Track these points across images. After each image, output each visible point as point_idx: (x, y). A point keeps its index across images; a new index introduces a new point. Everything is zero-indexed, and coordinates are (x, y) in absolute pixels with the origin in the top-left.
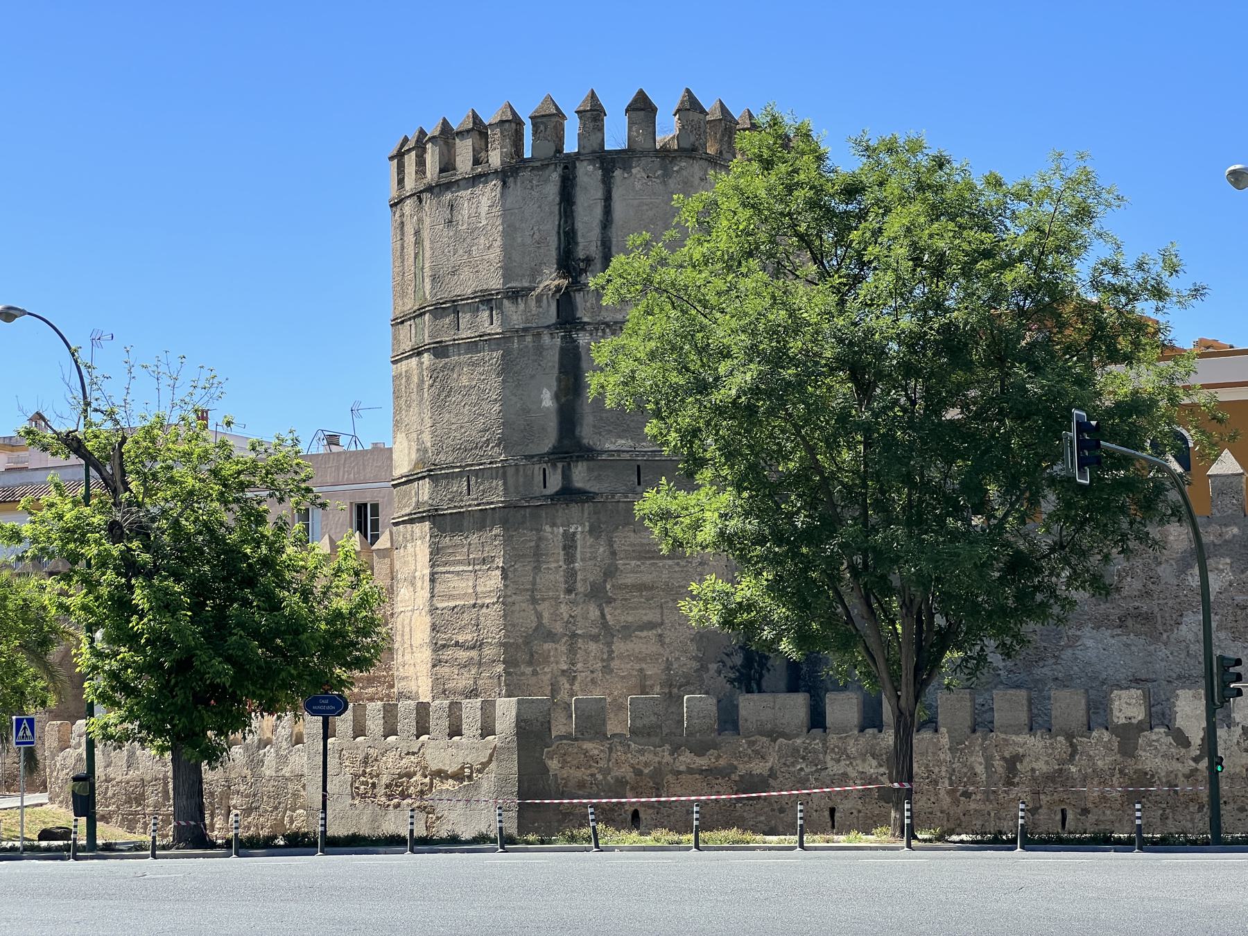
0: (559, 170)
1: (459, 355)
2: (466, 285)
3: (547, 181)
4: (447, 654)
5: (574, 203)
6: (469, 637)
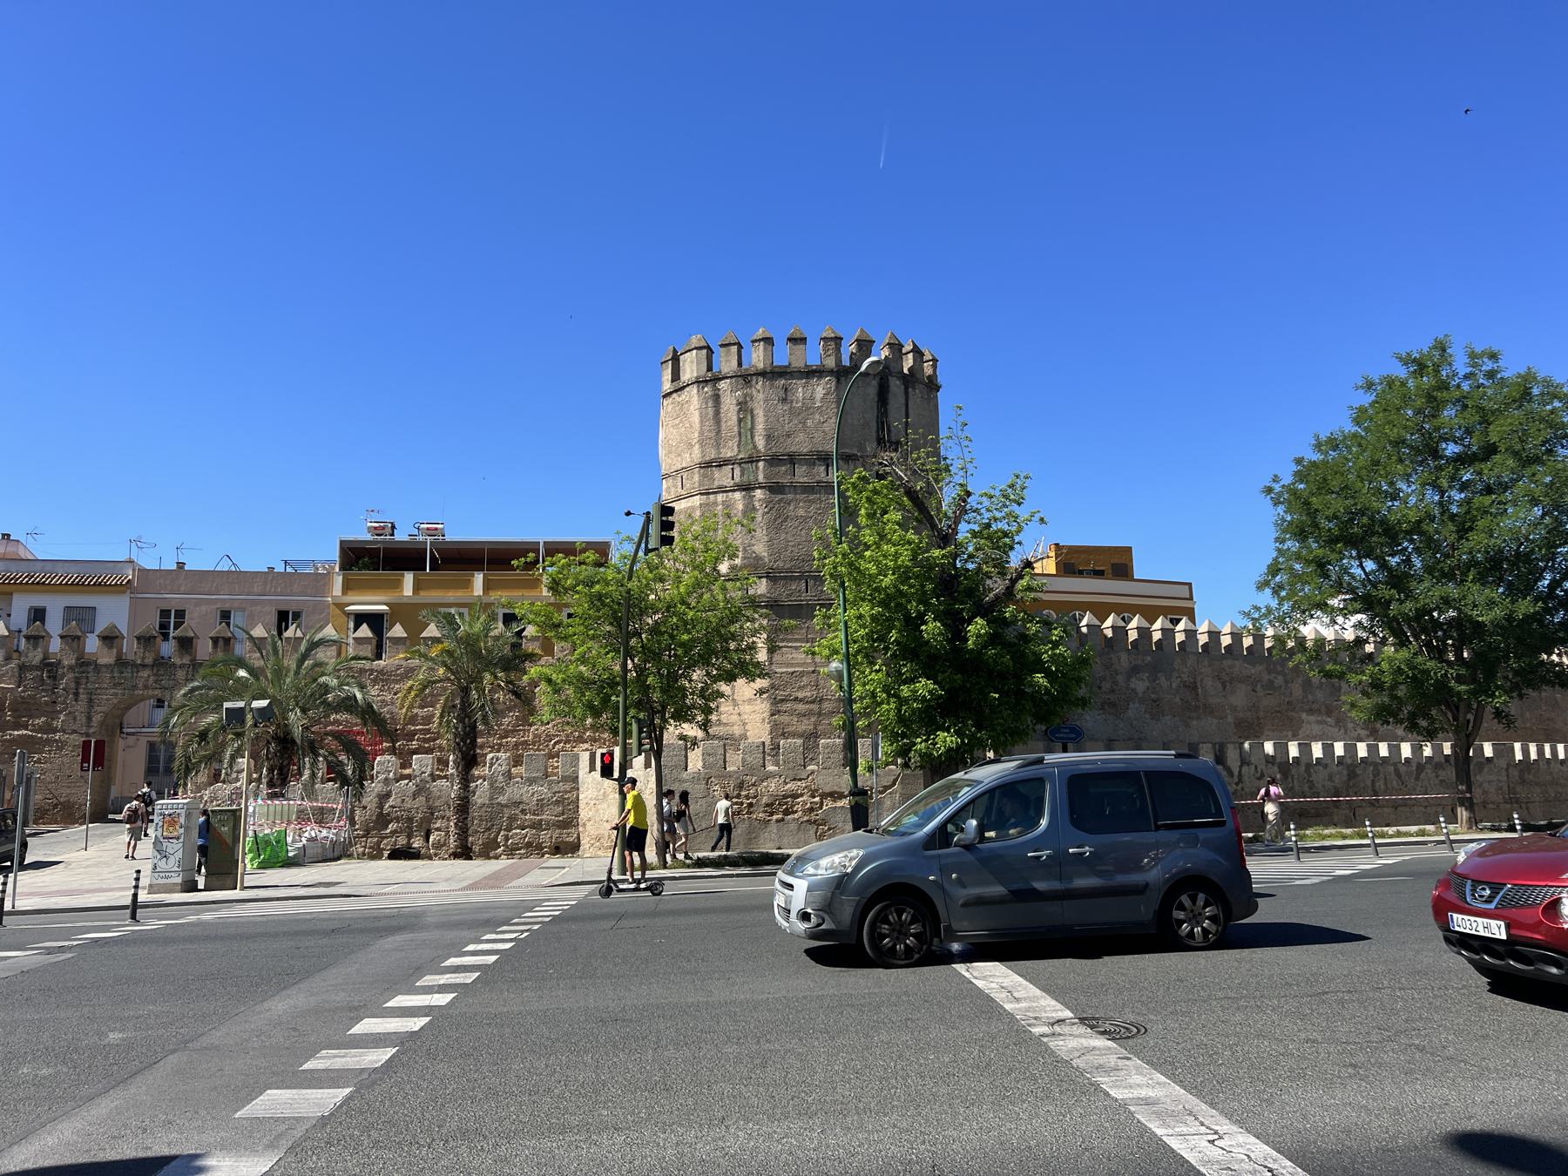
2: (800, 444)
4: (785, 707)
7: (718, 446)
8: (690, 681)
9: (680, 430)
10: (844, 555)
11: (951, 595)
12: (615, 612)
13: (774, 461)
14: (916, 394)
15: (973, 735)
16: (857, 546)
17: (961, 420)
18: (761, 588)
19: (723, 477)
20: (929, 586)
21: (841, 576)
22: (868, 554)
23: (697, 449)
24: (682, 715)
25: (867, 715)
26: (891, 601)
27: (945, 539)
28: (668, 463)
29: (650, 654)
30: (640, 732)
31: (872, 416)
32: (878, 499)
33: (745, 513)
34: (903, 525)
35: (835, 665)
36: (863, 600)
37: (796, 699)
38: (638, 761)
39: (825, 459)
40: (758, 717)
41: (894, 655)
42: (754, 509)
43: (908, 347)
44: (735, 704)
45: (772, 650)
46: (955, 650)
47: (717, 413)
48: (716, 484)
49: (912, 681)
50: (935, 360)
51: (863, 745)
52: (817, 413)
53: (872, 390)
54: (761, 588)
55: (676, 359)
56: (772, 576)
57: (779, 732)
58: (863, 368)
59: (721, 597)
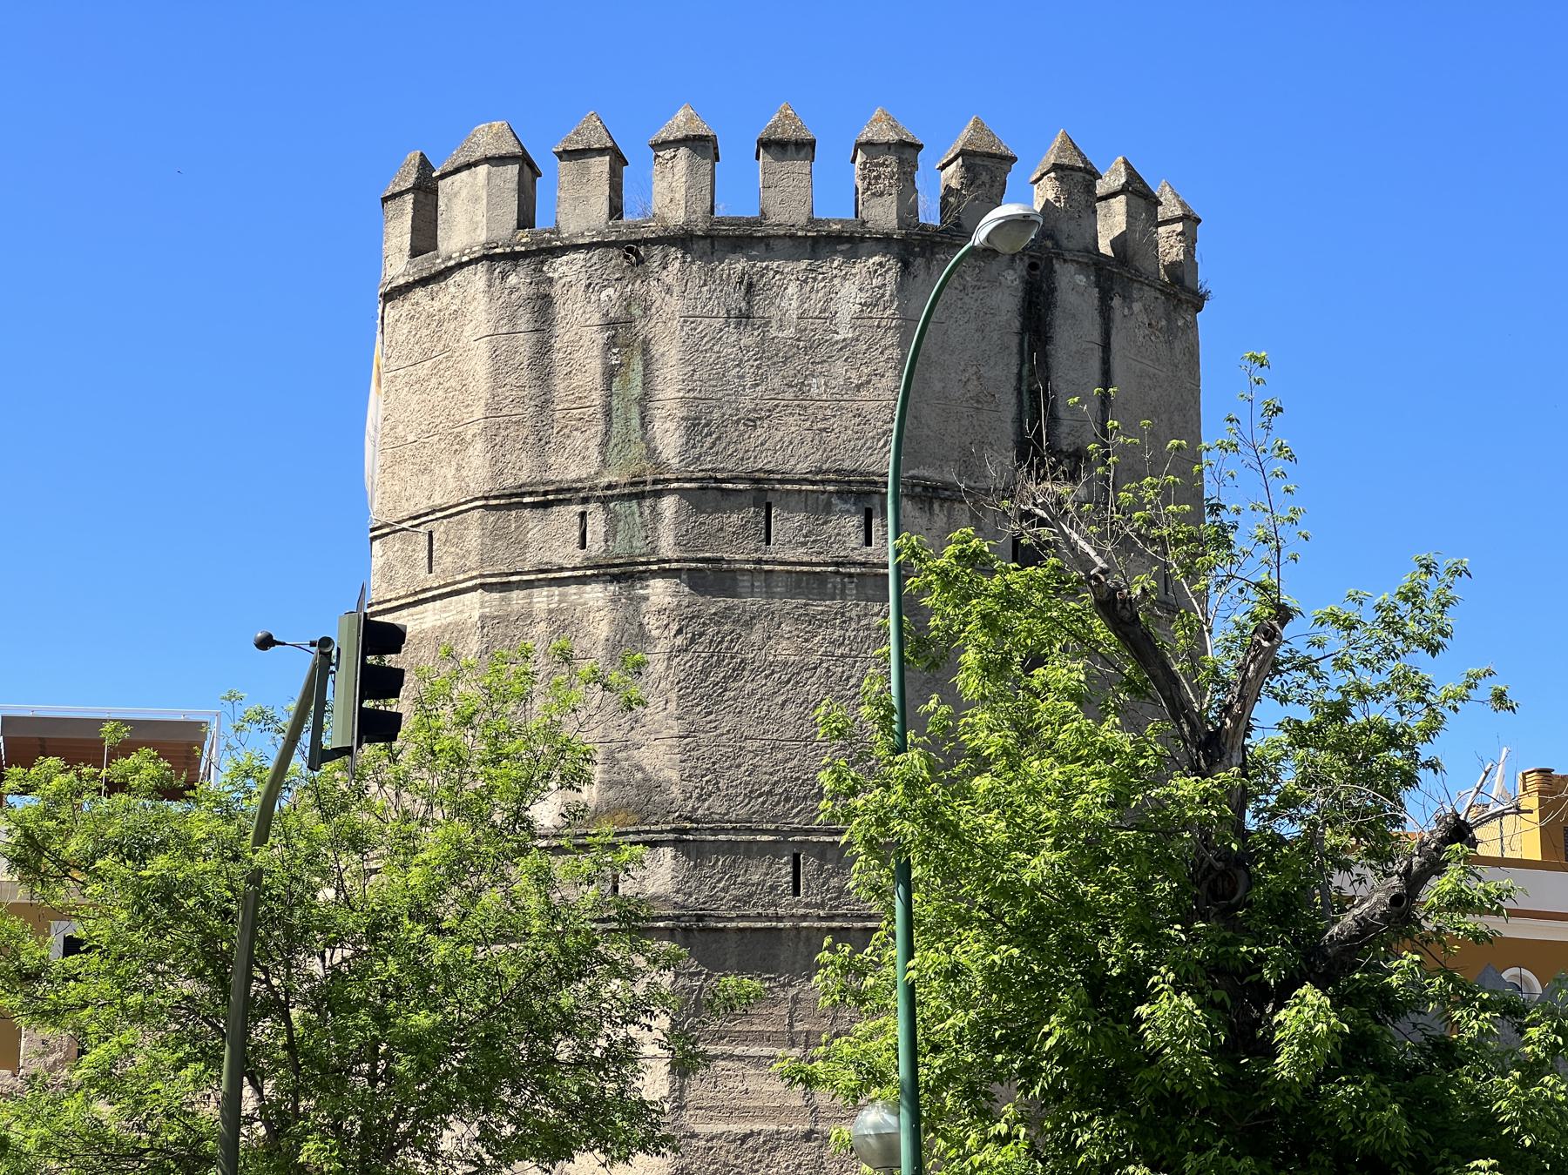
0: (1021, 267)
1: (770, 595)
2: (787, 448)
3: (995, 282)
7: (541, 444)
9: (432, 400)
11: (1226, 914)
12: (210, 939)
13: (708, 494)
14: (1135, 316)
16: (953, 759)
17: (1262, 396)
18: (657, 876)
19: (553, 538)
20: (1163, 887)
21: (900, 848)
22: (982, 783)
26: (1049, 926)
27: (1211, 746)
28: (389, 489)
31: (1003, 371)
36: (964, 921)
39: (860, 494)
41: (1054, 1093)
42: (643, 636)
43: (1112, 178)
47: (543, 349)
48: (531, 559)
50: (1190, 220)
52: (838, 365)
54: (657, 876)
55: (426, 190)
56: (689, 842)
58: (980, 236)
59: (533, 903)
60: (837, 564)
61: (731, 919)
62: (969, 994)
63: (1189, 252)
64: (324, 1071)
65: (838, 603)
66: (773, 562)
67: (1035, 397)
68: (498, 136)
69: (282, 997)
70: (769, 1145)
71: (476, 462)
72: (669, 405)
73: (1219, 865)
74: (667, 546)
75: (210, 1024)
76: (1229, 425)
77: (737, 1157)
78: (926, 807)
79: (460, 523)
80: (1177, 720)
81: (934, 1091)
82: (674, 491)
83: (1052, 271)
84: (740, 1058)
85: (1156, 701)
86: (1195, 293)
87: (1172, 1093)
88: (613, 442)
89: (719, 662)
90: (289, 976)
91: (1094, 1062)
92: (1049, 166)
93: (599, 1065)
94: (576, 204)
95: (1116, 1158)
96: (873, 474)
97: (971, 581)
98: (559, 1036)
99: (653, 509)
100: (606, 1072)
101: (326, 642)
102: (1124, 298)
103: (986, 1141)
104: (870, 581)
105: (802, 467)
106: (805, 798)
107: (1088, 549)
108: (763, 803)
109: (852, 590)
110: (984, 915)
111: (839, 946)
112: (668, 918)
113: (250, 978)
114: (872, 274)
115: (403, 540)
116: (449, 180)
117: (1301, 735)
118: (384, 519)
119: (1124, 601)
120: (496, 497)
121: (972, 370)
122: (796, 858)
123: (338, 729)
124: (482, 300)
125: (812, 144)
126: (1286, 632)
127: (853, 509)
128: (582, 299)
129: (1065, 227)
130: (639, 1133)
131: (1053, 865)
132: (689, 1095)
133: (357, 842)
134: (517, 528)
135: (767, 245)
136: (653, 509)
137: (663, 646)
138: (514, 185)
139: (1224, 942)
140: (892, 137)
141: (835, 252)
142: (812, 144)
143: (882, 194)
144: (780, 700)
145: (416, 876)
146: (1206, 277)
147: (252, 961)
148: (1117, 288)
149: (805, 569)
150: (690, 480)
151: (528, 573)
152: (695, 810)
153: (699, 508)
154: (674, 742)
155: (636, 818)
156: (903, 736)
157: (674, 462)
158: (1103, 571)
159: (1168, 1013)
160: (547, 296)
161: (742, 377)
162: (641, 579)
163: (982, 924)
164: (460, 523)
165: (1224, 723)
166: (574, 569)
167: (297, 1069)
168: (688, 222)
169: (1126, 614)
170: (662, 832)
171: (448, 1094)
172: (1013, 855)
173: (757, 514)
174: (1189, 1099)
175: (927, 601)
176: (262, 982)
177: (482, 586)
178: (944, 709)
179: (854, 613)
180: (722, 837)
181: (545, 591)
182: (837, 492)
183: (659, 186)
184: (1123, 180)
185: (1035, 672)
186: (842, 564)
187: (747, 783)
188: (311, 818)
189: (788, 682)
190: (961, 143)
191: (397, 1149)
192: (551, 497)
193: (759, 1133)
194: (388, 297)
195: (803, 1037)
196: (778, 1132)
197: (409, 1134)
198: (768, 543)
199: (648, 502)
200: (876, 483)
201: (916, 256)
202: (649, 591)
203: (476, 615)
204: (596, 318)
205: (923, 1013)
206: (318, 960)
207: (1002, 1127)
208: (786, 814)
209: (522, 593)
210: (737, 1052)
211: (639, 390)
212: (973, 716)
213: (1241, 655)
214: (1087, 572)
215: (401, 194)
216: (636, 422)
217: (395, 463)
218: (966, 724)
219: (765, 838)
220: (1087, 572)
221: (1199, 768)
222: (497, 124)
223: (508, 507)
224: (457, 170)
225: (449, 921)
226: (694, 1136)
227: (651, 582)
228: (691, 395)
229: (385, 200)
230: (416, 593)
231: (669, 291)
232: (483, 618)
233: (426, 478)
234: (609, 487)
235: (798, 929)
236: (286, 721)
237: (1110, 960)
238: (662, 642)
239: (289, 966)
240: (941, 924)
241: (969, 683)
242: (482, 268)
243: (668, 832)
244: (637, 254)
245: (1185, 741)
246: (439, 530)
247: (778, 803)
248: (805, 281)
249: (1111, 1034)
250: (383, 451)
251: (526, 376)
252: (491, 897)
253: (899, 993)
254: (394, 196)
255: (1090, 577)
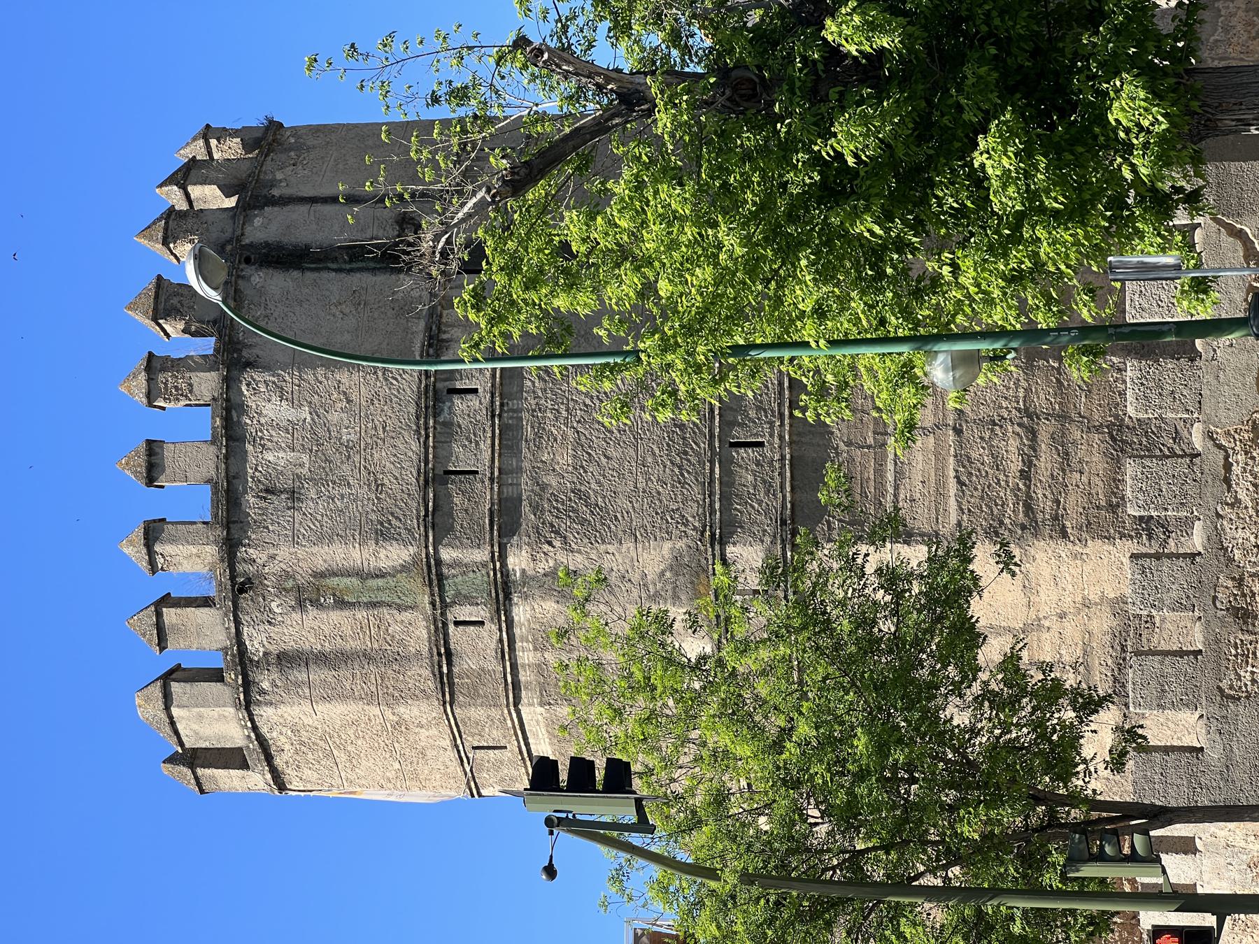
0: (248, 270)
1: (520, 470)
2: (400, 460)
3: (261, 292)
4: (1044, 503)
5: (308, 247)
6: (1013, 444)
7: (400, 659)
8: (974, 732)
9: (369, 749)
10: (667, 346)
11: (768, 86)
12: (800, 916)
13: (437, 522)
14: (288, 178)
15: (1117, 31)
16: (645, 314)
17: (341, 61)
18: (748, 556)
19: (476, 648)
20: (748, 139)
21: (718, 354)
22: (664, 288)
23: (413, 711)
24: (1062, 755)
25: (1066, 295)
26: (780, 236)
27: (630, 100)
28: (439, 783)
29: (903, 833)
30: (1101, 858)
31: (334, 284)
32: (533, 259)
33: (563, 596)
34: (594, 206)
35: (939, 372)
36: (778, 301)
37: (1025, 475)
38: (1178, 869)
39: (437, 396)
40: (1070, 570)
41: (918, 226)
42: (552, 574)
43: (174, 197)
44: (1034, 626)
45: (894, 528)
46: (904, 77)
47: (322, 659)
48: (493, 665)
49: (979, 180)
50: (207, 133)
51: (1145, 305)
52: (332, 416)
53: (271, 283)
54: (748, 556)
55: (193, 758)
56: (721, 533)
57: (1106, 519)
58: (214, 296)
59: (765, 654)
60: (493, 416)
61: (784, 497)
62: (838, 297)
63: (235, 133)
64: (907, 821)
65: (525, 415)
66: (492, 467)
67: (354, 257)
68: (148, 700)
69: (847, 856)
70: (966, 463)
71: (415, 712)
72: (366, 555)
73: (728, 92)
74: (481, 555)
75: (869, 914)
76: (367, 89)
77: (976, 489)
78: (684, 335)
79: (465, 724)
80: (610, 128)
81: (917, 324)
82: (435, 549)
83: (251, 245)
84: (897, 488)
85: (594, 146)
86: (267, 128)
87: (914, 130)
88: (398, 601)
89: (574, 511)
90: (829, 850)
91: (891, 193)
92: (164, 249)
93: (899, 596)
94: (202, 634)
95: (969, 176)
96: (419, 388)
97: (498, 299)
98: (876, 630)
99: (450, 566)
100: (904, 591)
101: (549, 822)
102: (272, 186)
103: (957, 283)
104: (506, 389)
105: (415, 446)
106: (684, 438)
107: (470, 204)
108: (689, 472)
109: (513, 404)
110: (773, 285)
111: (802, 404)
112: (784, 549)
113: (831, 881)
114: (256, 392)
115: (480, 771)
116: (184, 739)
117: (621, 28)
118: (464, 786)
119: (513, 173)
120: (444, 695)
121: (334, 310)
122: (733, 445)
123: (619, 810)
124: (283, 709)
125: (150, 443)
126: (537, 41)
127: (448, 404)
128: (281, 628)
129: (215, 235)
130: (954, 563)
131: (730, 229)
132: (927, 528)
133: (720, 799)
134: (468, 677)
135: (234, 477)
136: (450, 566)
137: (562, 557)
138: (188, 686)
139: (792, 91)
140: (142, 377)
141: (239, 422)
142: (150, 443)
143: (191, 385)
144: (604, 460)
145: (744, 750)
146: (254, 120)
147: (818, 881)
148: (265, 192)
149: (497, 442)
150: (427, 536)
151: (504, 667)
152: (695, 529)
153: (451, 529)
154: (640, 546)
155: (703, 576)
156: (627, 353)
157: (412, 550)
158: (488, 191)
159: (849, 140)
160: (278, 657)
161: (342, 496)
162: (508, 576)
163: (780, 287)
164: (465, 724)
165: (612, 90)
166: (500, 630)
167: (906, 842)
168: (216, 542)
169: (523, 172)
170: (714, 555)
171: (923, 719)
172: (723, 263)
173: (453, 482)
174: (919, 116)
175: (516, 334)
176: (835, 872)
177: (516, 705)
178: (606, 323)
179: (533, 402)
180: (717, 506)
181: (519, 654)
182: (435, 417)
183: (187, 567)
184: (175, 188)
185: (574, 249)
186: (493, 412)
187: (673, 486)
188: (701, 837)
189: (589, 454)
190: (147, 321)
191: (968, 760)
192: (443, 651)
193: (957, 471)
194: (282, 787)
195: (878, 437)
196: (956, 456)
197: (955, 750)
198: (476, 472)
199: (445, 571)
200: (426, 386)
201: (240, 356)
202: (517, 568)
203: (540, 709)
204: (296, 616)
205: (854, 334)
206: (817, 829)
207: (946, 270)
208: (698, 454)
209: (521, 672)
210: (891, 490)
211: (354, 579)
212: (610, 299)
213: (556, 77)
214: (489, 204)
215: (197, 778)
216: (380, 582)
217: (417, 778)
218: (617, 304)
219: (717, 470)
220: (489, 204)
221: (648, 110)
222: (138, 701)
223: (451, 685)
224: (176, 733)
225: (782, 722)
226: (959, 524)
227: (510, 567)
228: (357, 537)
229: (202, 791)
230: (523, 759)
231: (273, 557)
232: (542, 704)
233: (430, 753)
234: (433, 604)
235: (791, 443)
236: (624, 856)
237: (808, 181)
238: (558, 557)
239: (822, 851)
240: (780, 319)
241: (581, 303)
242: (256, 711)
243: (713, 550)
244: (243, 584)
245: (627, 122)
246: (471, 741)
247: (688, 460)
248: (263, 446)
249: (868, 182)
250: (408, 789)
251: (344, 673)
252: (762, 689)
253: (838, 353)
254: (199, 784)
255: (493, 201)
